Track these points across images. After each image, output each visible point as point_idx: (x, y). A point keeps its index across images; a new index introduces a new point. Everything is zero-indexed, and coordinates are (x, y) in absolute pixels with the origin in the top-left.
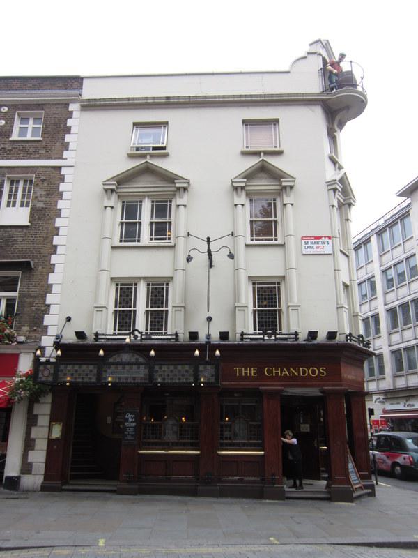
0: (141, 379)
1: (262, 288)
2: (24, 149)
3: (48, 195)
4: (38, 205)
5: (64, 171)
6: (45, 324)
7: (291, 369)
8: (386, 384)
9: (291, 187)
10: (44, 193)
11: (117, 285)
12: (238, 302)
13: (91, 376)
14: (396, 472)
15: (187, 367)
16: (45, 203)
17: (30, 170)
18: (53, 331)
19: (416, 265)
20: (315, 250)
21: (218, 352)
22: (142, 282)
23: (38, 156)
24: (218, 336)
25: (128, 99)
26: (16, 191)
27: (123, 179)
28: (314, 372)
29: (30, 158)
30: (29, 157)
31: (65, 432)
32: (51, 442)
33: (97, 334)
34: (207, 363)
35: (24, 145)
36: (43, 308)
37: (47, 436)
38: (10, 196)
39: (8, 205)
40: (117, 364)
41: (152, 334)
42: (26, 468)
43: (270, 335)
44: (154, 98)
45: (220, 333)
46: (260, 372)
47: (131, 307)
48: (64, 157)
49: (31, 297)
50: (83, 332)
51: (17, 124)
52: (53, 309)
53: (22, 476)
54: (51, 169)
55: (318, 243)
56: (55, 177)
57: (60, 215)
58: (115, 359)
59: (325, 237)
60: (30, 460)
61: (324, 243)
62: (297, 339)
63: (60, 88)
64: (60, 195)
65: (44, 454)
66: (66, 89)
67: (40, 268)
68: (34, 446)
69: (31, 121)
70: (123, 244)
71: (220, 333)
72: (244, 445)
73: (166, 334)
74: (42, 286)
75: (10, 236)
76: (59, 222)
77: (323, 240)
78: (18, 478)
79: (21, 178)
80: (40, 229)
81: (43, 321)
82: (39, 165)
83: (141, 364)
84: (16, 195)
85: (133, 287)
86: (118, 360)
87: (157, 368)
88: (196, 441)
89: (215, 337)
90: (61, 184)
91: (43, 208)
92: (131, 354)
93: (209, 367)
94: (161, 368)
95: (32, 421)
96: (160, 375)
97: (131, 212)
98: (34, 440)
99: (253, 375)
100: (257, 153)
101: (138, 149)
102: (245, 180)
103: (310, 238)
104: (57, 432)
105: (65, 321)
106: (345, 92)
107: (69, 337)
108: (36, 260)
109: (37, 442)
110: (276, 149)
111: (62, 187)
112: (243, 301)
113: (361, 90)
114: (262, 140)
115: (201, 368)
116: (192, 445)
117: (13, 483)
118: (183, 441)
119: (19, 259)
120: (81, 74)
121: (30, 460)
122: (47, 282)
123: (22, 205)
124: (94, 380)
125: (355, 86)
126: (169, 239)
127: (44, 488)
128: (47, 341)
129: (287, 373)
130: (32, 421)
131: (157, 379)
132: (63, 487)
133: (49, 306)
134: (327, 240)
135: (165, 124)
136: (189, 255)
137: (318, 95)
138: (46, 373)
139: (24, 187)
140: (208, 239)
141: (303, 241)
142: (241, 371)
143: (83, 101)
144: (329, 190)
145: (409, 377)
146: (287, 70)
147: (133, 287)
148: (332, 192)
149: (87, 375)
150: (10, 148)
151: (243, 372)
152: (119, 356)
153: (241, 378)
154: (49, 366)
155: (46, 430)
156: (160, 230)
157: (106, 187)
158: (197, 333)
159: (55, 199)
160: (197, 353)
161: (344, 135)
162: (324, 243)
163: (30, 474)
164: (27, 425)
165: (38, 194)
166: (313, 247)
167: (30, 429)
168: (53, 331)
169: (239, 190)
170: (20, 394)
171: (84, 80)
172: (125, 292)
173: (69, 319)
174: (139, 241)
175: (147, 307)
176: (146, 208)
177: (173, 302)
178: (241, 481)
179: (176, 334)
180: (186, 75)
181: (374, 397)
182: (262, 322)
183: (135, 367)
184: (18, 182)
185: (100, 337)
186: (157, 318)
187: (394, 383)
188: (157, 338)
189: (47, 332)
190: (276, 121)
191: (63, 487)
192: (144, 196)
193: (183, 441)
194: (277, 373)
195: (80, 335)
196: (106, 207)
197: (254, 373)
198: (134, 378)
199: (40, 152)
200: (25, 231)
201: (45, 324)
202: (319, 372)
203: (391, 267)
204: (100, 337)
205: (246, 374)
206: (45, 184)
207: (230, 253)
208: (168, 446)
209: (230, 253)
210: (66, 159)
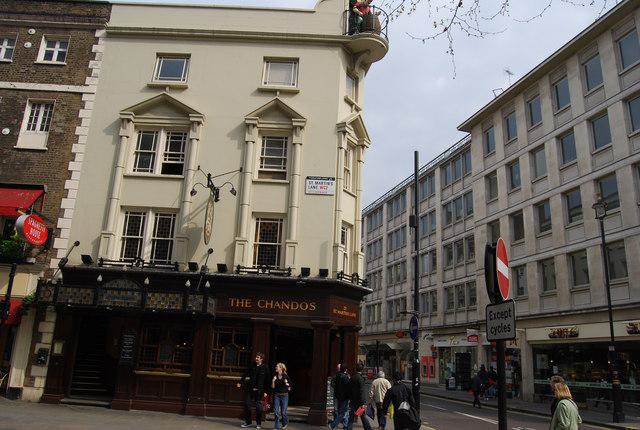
2: (46, 73)
3: (68, 120)
5: (85, 97)
6: (55, 247)
8: (437, 321)
9: (302, 128)
12: (289, 238)
16: (64, 128)
18: (61, 254)
20: (318, 190)
21: (208, 284)
24: (216, 268)
25: (154, 29)
26: (37, 114)
27: (139, 110)
35: (48, 68)
39: (28, 129)
43: (264, 269)
45: (320, 270)
51: (43, 47)
62: (289, 274)
64: (79, 121)
69: (57, 46)
70: (163, 176)
71: (320, 270)
73: (169, 263)
79: (43, 102)
82: (38, 89)
83: (136, 290)
84: (36, 119)
85: (142, 216)
89: (213, 269)
90: (81, 111)
97: (147, 141)
100: (273, 92)
103: (316, 178)
106: (367, 37)
107: (75, 260)
111: (82, 113)
113: (383, 36)
114: (277, 79)
115: (191, 297)
117: (16, 393)
123: (42, 129)
125: (378, 31)
127: (43, 400)
128: (54, 264)
140: (209, 175)
141: (308, 181)
142: (235, 302)
143: (108, 28)
145: (458, 315)
146: (312, 8)
147: (142, 216)
149: (173, 303)
153: (235, 309)
157: (123, 117)
160: (188, 283)
161: (367, 80)
168: (61, 254)
171: (113, 7)
172: (134, 221)
174: (151, 171)
176: (163, 138)
177: (178, 233)
179: (290, 269)
181: (423, 334)
184: (39, 106)
187: (445, 320)
188: (160, 268)
190: (296, 61)
192: (160, 128)
194: (269, 306)
195: (86, 259)
201: (55, 247)
203: (380, 208)
205: (240, 305)
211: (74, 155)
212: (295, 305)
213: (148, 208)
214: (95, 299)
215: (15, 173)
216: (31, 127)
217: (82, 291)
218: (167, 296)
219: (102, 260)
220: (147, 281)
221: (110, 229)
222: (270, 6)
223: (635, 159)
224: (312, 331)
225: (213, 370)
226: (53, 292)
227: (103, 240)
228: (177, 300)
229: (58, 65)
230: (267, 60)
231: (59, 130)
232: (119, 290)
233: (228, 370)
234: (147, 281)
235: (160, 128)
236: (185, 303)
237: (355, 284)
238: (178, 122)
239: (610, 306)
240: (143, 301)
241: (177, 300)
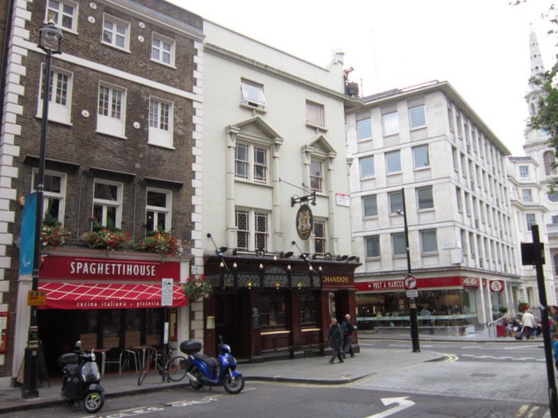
3: (185, 124)
10: (182, 121)
14: (224, 363)
15: (256, 276)
17: (106, 76)
23: (174, 84)
25: (241, 57)
29: (167, 84)
30: (97, 60)
37: (202, 327)
38: (59, 91)
40: (271, 274)
44: (258, 63)
49: (181, 214)
52: (197, 226)
54: (186, 101)
63: (185, 22)
66: (191, 25)
72: (310, 325)
74: (188, 206)
86: (271, 272)
87: (239, 276)
93: (230, 275)
95: (192, 316)
97: (241, 152)
98: (194, 331)
101: (250, 103)
102: (239, 129)
104: (211, 325)
110: (262, 110)
116: (284, 327)
120: (203, 16)
126: (265, 180)
130: (192, 316)
133: (194, 223)
135: (261, 86)
137: (341, 95)
138: (229, 280)
139: (58, 82)
144: (303, 153)
148: (305, 154)
155: (202, 323)
156: (259, 171)
169: (233, 135)
170: (203, 295)
178: (276, 351)
180: (273, 48)
186: (261, 239)
188: (320, 258)
189: (194, 245)
192: (250, 143)
200: (170, 153)
208: (273, 328)
210: (195, 94)
211: (194, 157)
213: (251, 208)
214: (262, 282)
215: (152, 169)
222: (276, 47)
229: (116, 50)
230: (308, 102)
232: (275, 275)
235: (250, 143)
236: (262, 282)
238: (265, 141)
239: (409, 270)
240: (235, 281)
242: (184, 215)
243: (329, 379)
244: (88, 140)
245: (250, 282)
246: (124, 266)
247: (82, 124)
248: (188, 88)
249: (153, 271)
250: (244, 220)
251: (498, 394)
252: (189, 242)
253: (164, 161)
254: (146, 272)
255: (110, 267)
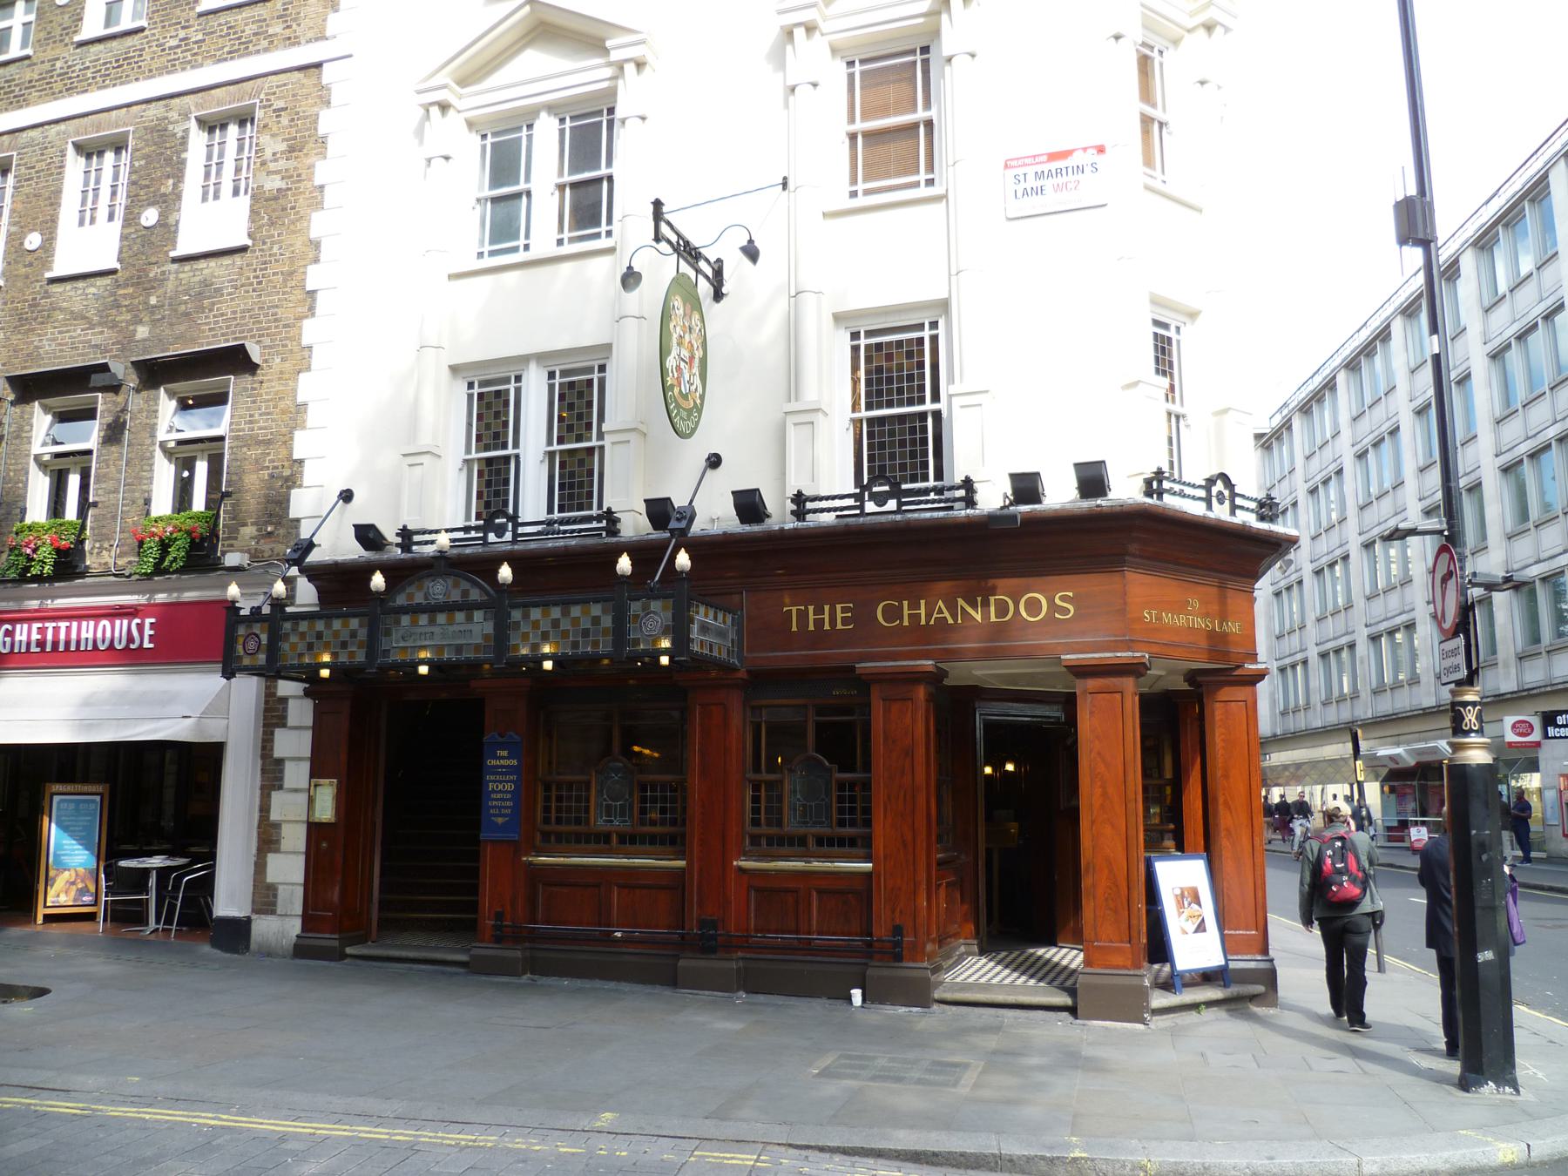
0: (477, 647)
1: (879, 346)
3: (293, 150)
4: (267, 187)
6: (292, 515)
7: (961, 602)
10: (283, 147)
11: (471, 385)
13: (354, 649)
19: (1480, 483)
20: (1050, 200)
22: (533, 366)
28: (1033, 606)
29: (186, 65)
31: (345, 801)
32: (315, 830)
33: (406, 534)
34: (653, 595)
36: (287, 473)
37: (305, 819)
40: (415, 610)
41: (562, 522)
42: (265, 898)
46: (862, 616)
47: (505, 446)
48: (328, 34)
49: (259, 443)
50: (372, 527)
52: (309, 475)
53: (254, 917)
55: (1059, 172)
56: (307, 97)
57: (322, 202)
58: (410, 597)
59: (1085, 149)
60: (271, 878)
61: (1080, 169)
62: (970, 502)
65: (300, 862)
67: (278, 360)
68: (278, 842)
74: (283, 412)
75: (206, 283)
76: (318, 225)
77: (1077, 159)
78: (248, 921)
80: (275, 249)
81: (288, 508)
86: (419, 598)
87: (516, 615)
88: (672, 829)
91: (279, 190)
92: (450, 581)
93: (655, 605)
94: (526, 616)
96: (525, 636)
98: (277, 826)
99: (839, 626)
104: (325, 811)
105: (336, 499)
108: (267, 341)
109: (286, 831)
112: (810, 394)
117: (234, 934)
118: (647, 829)
119: (227, 341)
121: (271, 878)
122: (295, 397)
124: (360, 657)
127: (301, 950)
129: (947, 614)
131: (516, 648)
132: (349, 950)
133: (301, 462)
134: (1091, 156)
136: (630, 268)
142: (803, 616)
149: (586, 633)
150: (200, 37)
151: (811, 617)
152: (420, 588)
154: (257, 629)
155: (303, 798)
158: (1035, 477)
159: (308, 161)
162: (1080, 169)
163: (273, 912)
164: (262, 788)
165: (268, 154)
166: (1040, 191)
167: (269, 796)
173: (347, 496)
174: (527, 247)
175: (550, 443)
182: (571, 486)
183: (460, 616)
185: (809, 505)
191: (349, 950)
193: (647, 829)
196: (429, 161)
197: (845, 621)
198: (459, 649)
199: (271, 31)
201: (292, 515)
202: (1053, 606)
204: (809, 505)
205: (819, 611)
206: (285, 121)
207: (751, 241)
208: (602, 841)
209: (751, 241)
211: (316, 245)
212: (1159, 618)
213: (525, 359)
214: (371, 645)
216: (210, 192)
217: (576, 611)
218: (565, 613)
219: (799, 499)
220: (505, 573)
221: (810, 395)
223: (821, 4)
224: (1069, 702)
225: (755, 840)
226: (264, 638)
227: (792, 433)
228: (353, 634)
231: (273, 184)
233: (802, 841)
234: (505, 573)
237: (1221, 513)
241: (596, 621)
242: (269, 443)
243: (1200, 791)
244: (34, 305)
245: (326, 647)
246: (75, 624)
247: (23, 271)
248: (310, 35)
249: (148, 632)
250: (500, 414)
251: (200, 61)
252: (282, 531)
253: (218, 290)
254: (130, 639)
255: (42, 631)
